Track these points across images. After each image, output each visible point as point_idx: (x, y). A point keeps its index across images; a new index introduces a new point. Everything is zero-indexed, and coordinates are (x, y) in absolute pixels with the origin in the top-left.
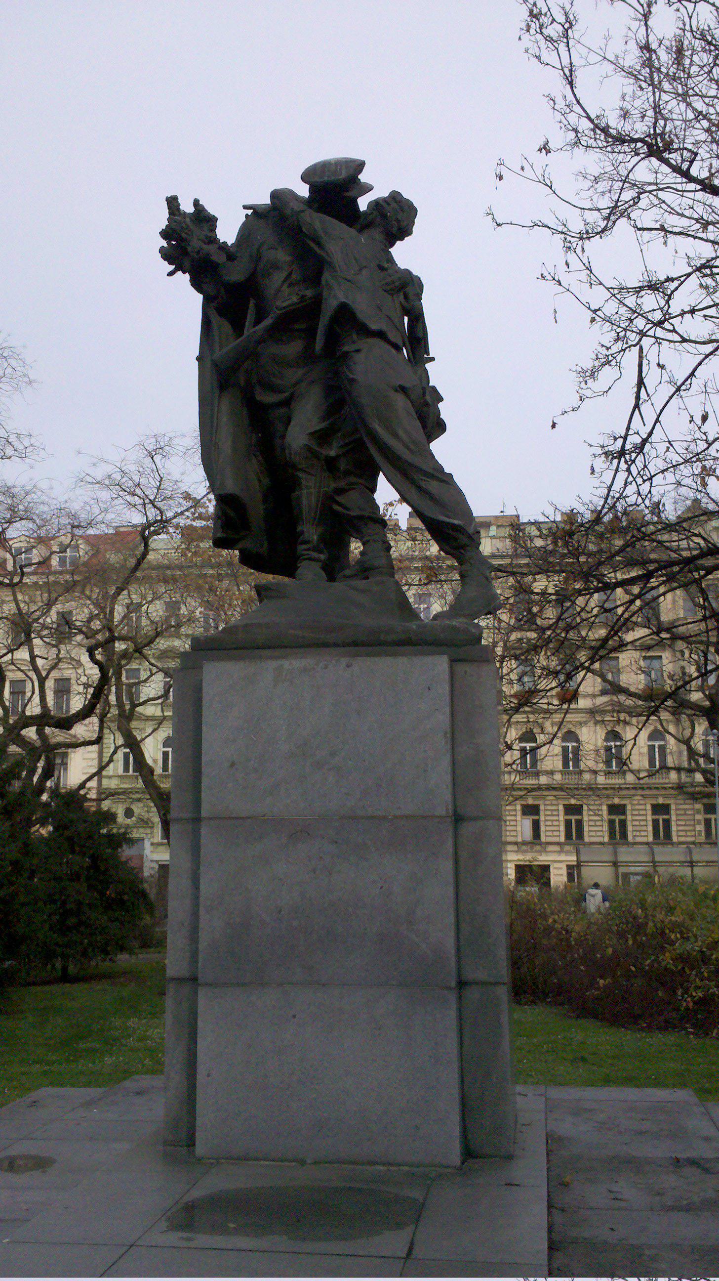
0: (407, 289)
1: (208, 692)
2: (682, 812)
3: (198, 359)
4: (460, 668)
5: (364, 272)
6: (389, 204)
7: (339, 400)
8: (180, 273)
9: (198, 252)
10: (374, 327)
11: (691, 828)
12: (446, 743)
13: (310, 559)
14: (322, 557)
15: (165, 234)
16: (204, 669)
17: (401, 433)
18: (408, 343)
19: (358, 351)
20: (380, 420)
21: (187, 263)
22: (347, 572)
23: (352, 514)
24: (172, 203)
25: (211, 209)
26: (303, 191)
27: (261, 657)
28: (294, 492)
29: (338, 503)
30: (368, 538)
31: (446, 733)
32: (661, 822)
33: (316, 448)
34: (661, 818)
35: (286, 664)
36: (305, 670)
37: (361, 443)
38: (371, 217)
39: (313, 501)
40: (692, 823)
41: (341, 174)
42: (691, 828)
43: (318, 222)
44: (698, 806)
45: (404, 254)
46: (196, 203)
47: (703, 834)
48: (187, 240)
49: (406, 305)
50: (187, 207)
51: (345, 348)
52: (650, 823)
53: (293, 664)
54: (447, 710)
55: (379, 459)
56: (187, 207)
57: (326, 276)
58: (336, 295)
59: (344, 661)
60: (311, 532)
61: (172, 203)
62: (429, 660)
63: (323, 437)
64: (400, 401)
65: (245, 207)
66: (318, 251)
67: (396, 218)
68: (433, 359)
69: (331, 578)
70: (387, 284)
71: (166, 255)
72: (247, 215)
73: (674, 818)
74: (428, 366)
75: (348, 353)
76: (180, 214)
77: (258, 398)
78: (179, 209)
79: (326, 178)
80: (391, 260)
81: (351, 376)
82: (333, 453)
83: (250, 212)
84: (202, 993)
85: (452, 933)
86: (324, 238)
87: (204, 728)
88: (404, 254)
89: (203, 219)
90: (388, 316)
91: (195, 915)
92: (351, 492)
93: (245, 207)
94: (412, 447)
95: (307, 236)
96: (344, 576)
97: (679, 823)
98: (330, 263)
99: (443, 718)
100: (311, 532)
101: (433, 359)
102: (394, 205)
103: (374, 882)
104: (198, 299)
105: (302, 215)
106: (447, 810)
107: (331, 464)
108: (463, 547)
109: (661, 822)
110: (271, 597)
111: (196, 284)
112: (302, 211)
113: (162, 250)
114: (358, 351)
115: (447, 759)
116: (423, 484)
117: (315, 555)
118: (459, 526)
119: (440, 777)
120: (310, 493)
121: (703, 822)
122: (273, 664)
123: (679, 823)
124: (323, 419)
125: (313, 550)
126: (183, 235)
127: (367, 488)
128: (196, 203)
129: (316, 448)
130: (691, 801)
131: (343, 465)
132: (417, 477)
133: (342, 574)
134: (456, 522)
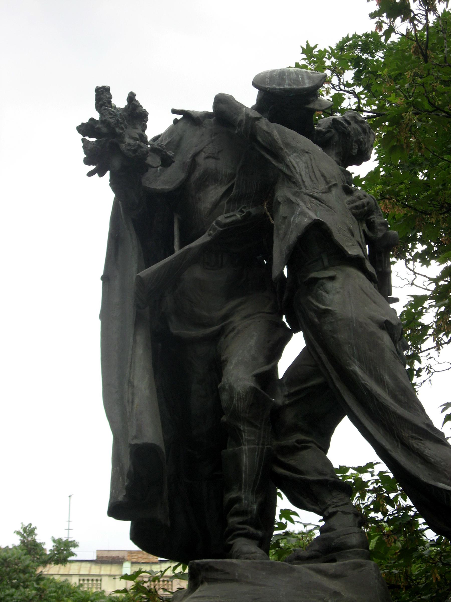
3: (103, 278)
5: (334, 190)
6: (349, 123)
9: (135, 151)
15: (86, 129)
17: (387, 378)
19: (332, 278)
20: (360, 360)
21: (117, 163)
24: (103, 96)
26: (248, 98)
28: (225, 448)
30: (331, 510)
38: (329, 135)
41: (304, 83)
43: (279, 132)
46: (131, 98)
48: (113, 138)
49: (370, 234)
50: (119, 101)
56: (119, 101)
57: (283, 192)
61: (103, 96)
65: (174, 111)
70: (357, 207)
72: (176, 121)
75: (316, 280)
76: (111, 107)
78: (110, 102)
79: (287, 87)
81: (323, 307)
83: (179, 117)
86: (285, 150)
89: (135, 114)
92: (304, 453)
93: (174, 111)
105: (257, 123)
110: (215, 581)
116: (415, 443)
125: (251, 525)
126: (118, 130)
128: (131, 98)
131: (289, 417)
132: (406, 434)
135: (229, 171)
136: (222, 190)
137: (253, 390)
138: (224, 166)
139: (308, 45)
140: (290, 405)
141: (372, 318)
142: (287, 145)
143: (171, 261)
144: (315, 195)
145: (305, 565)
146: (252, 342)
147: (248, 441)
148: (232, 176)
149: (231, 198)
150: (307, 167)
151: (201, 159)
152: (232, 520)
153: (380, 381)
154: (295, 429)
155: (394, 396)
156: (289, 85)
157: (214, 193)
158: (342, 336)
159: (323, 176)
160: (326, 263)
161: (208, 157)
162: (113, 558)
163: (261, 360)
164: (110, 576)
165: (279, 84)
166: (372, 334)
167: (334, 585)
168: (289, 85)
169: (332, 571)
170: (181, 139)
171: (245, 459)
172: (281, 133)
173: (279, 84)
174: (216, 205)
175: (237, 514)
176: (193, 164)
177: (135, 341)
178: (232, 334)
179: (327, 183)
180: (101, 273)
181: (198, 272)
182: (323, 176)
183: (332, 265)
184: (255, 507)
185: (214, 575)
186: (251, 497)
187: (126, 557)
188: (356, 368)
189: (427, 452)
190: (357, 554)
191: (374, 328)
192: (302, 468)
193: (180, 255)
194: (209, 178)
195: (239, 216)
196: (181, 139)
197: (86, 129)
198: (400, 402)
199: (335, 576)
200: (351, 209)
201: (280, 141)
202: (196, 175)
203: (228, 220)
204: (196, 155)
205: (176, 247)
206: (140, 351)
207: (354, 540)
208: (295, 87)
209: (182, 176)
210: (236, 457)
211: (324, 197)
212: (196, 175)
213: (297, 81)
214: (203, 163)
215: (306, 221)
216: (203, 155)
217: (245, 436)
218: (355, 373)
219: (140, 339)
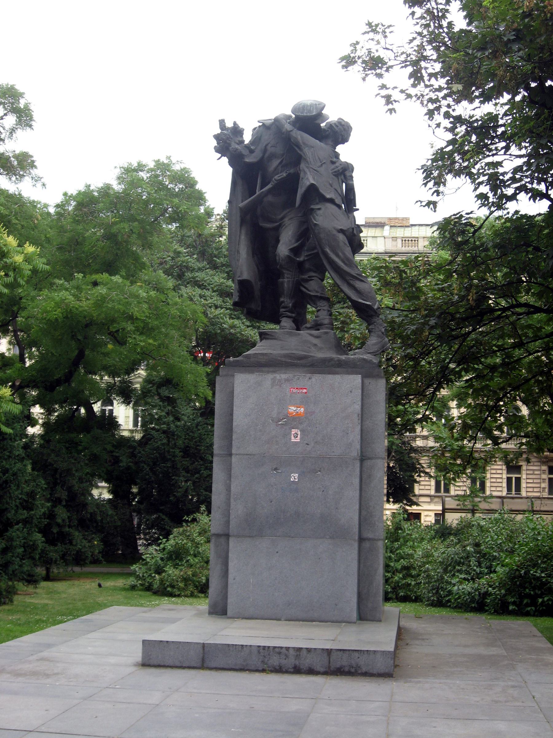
0: (344, 173)
1: (237, 390)
2: (531, 472)
4: (367, 381)
7: (306, 232)
8: (223, 157)
9: (235, 151)
10: (328, 196)
11: (538, 485)
12: (359, 420)
13: (287, 317)
14: (293, 315)
15: (217, 137)
16: (236, 377)
17: (340, 254)
18: (345, 201)
19: (319, 209)
20: (329, 246)
22: (308, 325)
23: (312, 294)
24: (222, 123)
25: (241, 126)
27: (263, 372)
29: (305, 288)
31: (358, 415)
32: (514, 479)
33: (293, 256)
34: (514, 476)
35: (278, 376)
36: (287, 380)
37: (317, 254)
39: (291, 285)
40: (538, 481)
42: (538, 485)
44: (545, 468)
45: (345, 152)
47: (547, 490)
51: (312, 207)
52: (505, 481)
53: (282, 376)
54: (360, 403)
55: (328, 266)
57: (303, 165)
58: (309, 178)
59: (309, 375)
60: (287, 301)
62: (352, 377)
63: (296, 251)
64: (341, 237)
65: (259, 122)
66: (299, 151)
67: (340, 133)
68: (358, 210)
69: (298, 329)
70: (335, 172)
71: (217, 150)
73: (524, 476)
74: (355, 213)
75: (313, 209)
77: (261, 224)
78: (225, 126)
79: (305, 114)
80: (337, 155)
81: (315, 222)
82: (301, 259)
84: (232, 542)
85: (357, 514)
87: (235, 408)
88: (345, 152)
89: (237, 131)
90: (336, 190)
91: (228, 504)
92: (311, 282)
94: (346, 262)
95: (293, 143)
96: (306, 327)
97: (528, 481)
98: (305, 159)
99: (357, 407)
100: (287, 301)
101: (358, 210)
102: (340, 127)
103: (319, 488)
104: (230, 170)
105: (291, 133)
106: (358, 453)
107: (300, 265)
108: (372, 316)
109: (514, 479)
111: (231, 163)
112: (291, 131)
113: (215, 147)
114: (319, 209)
115: (359, 427)
116: (351, 282)
117: (289, 314)
118: (369, 305)
119: (355, 436)
120: (287, 281)
121: (547, 481)
122: (270, 376)
123: (528, 481)
124: (297, 241)
127: (320, 279)
128: (235, 123)
129: (293, 256)
130: (539, 464)
131: (307, 266)
132: (348, 278)
133: (304, 326)
134: (368, 303)
135: (282, 152)
136: (279, 161)
137: (288, 257)
138: (279, 150)
139: (368, 21)
140: (307, 260)
141: (334, 228)
142: (304, 143)
143: (254, 198)
144: (315, 169)
145: (306, 331)
146: (290, 233)
147: (288, 278)
148: (283, 155)
149: (283, 166)
150: (312, 155)
151: (269, 147)
152: (282, 310)
153: (338, 256)
154: (310, 270)
155: (343, 262)
156: (306, 113)
157: (275, 163)
158: (322, 236)
159: (319, 158)
160: (317, 201)
161: (272, 147)
162: (377, 223)
163: (293, 241)
164: (373, 237)
165: (302, 113)
166: (334, 235)
167: (315, 341)
168: (306, 113)
169: (316, 335)
170: (261, 136)
171: (286, 285)
172: (302, 137)
173: (302, 113)
174: (276, 169)
175: (284, 307)
176: (265, 151)
177: (240, 232)
178: (284, 227)
179: (321, 162)
180: (228, 198)
181: (270, 198)
182: (319, 158)
183: (320, 202)
184: (291, 305)
185: (267, 336)
186: (289, 301)
187: (387, 223)
188: (328, 250)
189: (357, 286)
190: (327, 328)
191: (335, 232)
192: (309, 289)
193: (259, 195)
194: (273, 156)
195: (285, 175)
196: (261, 136)
197: (217, 137)
198: (345, 264)
199: (317, 337)
200: (332, 173)
201: (301, 142)
202: (267, 155)
203: (279, 178)
204: (267, 145)
205: (257, 191)
206: (243, 237)
207: (326, 321)
208: (308, 114)
209: (261, 155)
210: (282, 283)
211: (318, 169)
212: (267, 155)
213: (310, 111)
214: (270, 150)
215: (308, 184)
216: (270, 145)
217: (286, 275)
218: (327, 252)
219: (243, 232)
